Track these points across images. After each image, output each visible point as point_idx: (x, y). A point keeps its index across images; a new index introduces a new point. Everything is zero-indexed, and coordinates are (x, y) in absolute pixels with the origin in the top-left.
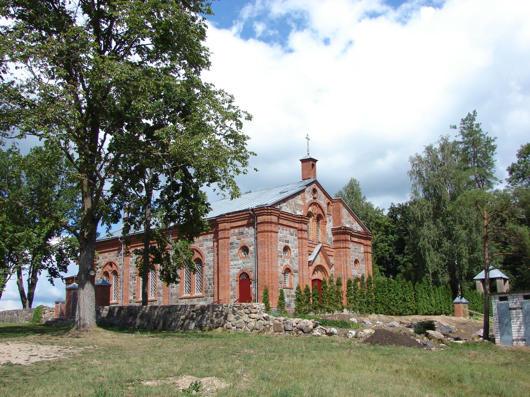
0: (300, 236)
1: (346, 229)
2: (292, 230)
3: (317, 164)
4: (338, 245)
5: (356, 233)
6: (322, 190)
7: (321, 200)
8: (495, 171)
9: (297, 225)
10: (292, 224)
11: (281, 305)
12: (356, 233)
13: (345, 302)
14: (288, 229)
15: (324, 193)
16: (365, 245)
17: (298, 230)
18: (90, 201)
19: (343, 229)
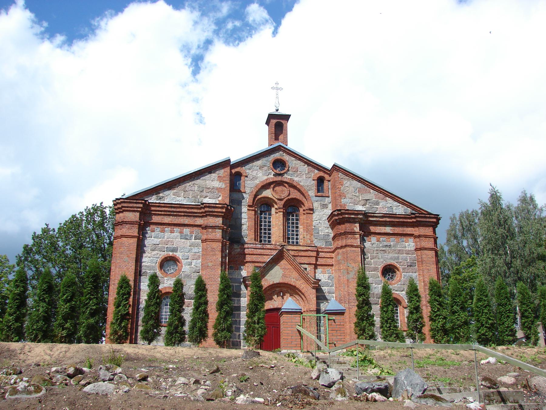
0: (204, 237)
1: (342, 214)
2: (187, 230)
3: (290, 126)
4: (340, 243)
5: (382, 217)
6: (300, 160)
7: (300, 175)
8: (32, 27)
9: (199, 221)
10: (186, 221)
11: (389, 321)
12: (382, 217)
13: (426, 330)
14: (176, 229)
15: (305, 163)
16: (415, 237)
17: (203, 228)
18: (390, 199)
19: (338, 215)
